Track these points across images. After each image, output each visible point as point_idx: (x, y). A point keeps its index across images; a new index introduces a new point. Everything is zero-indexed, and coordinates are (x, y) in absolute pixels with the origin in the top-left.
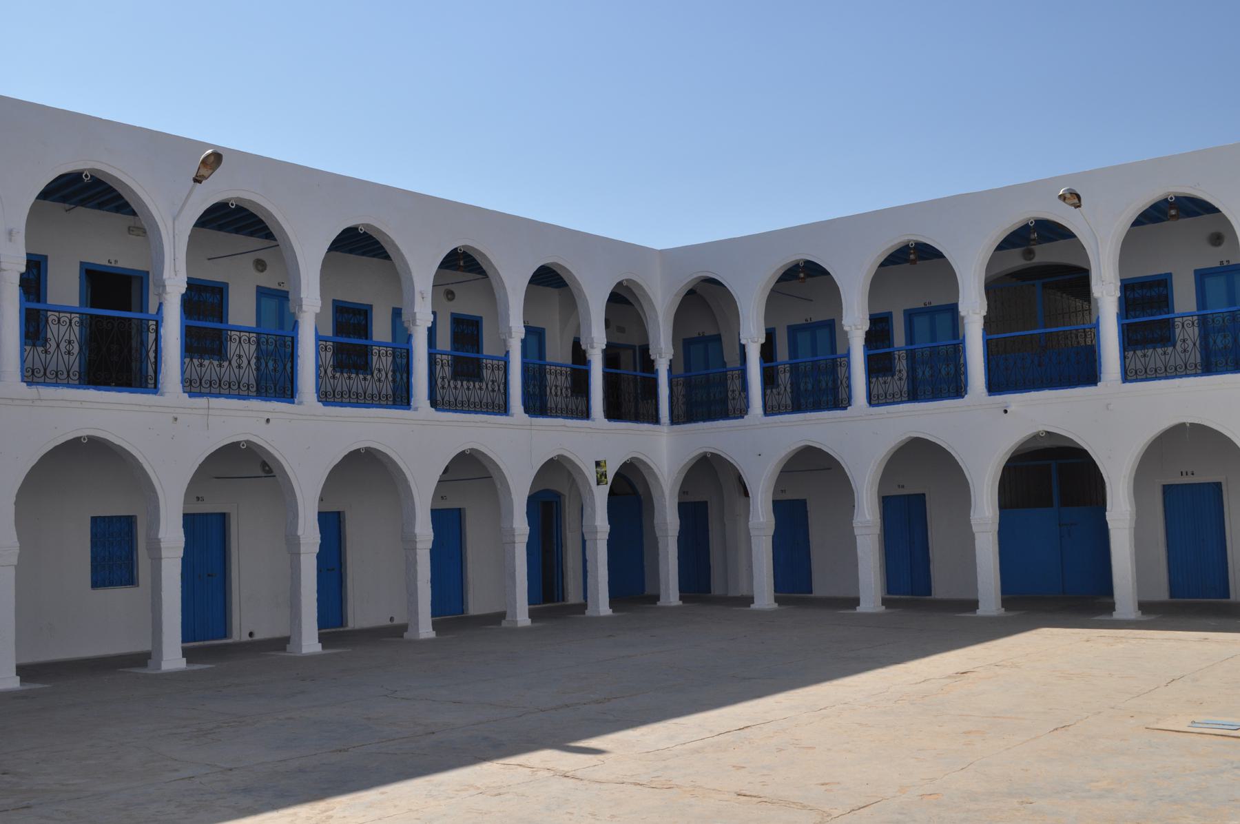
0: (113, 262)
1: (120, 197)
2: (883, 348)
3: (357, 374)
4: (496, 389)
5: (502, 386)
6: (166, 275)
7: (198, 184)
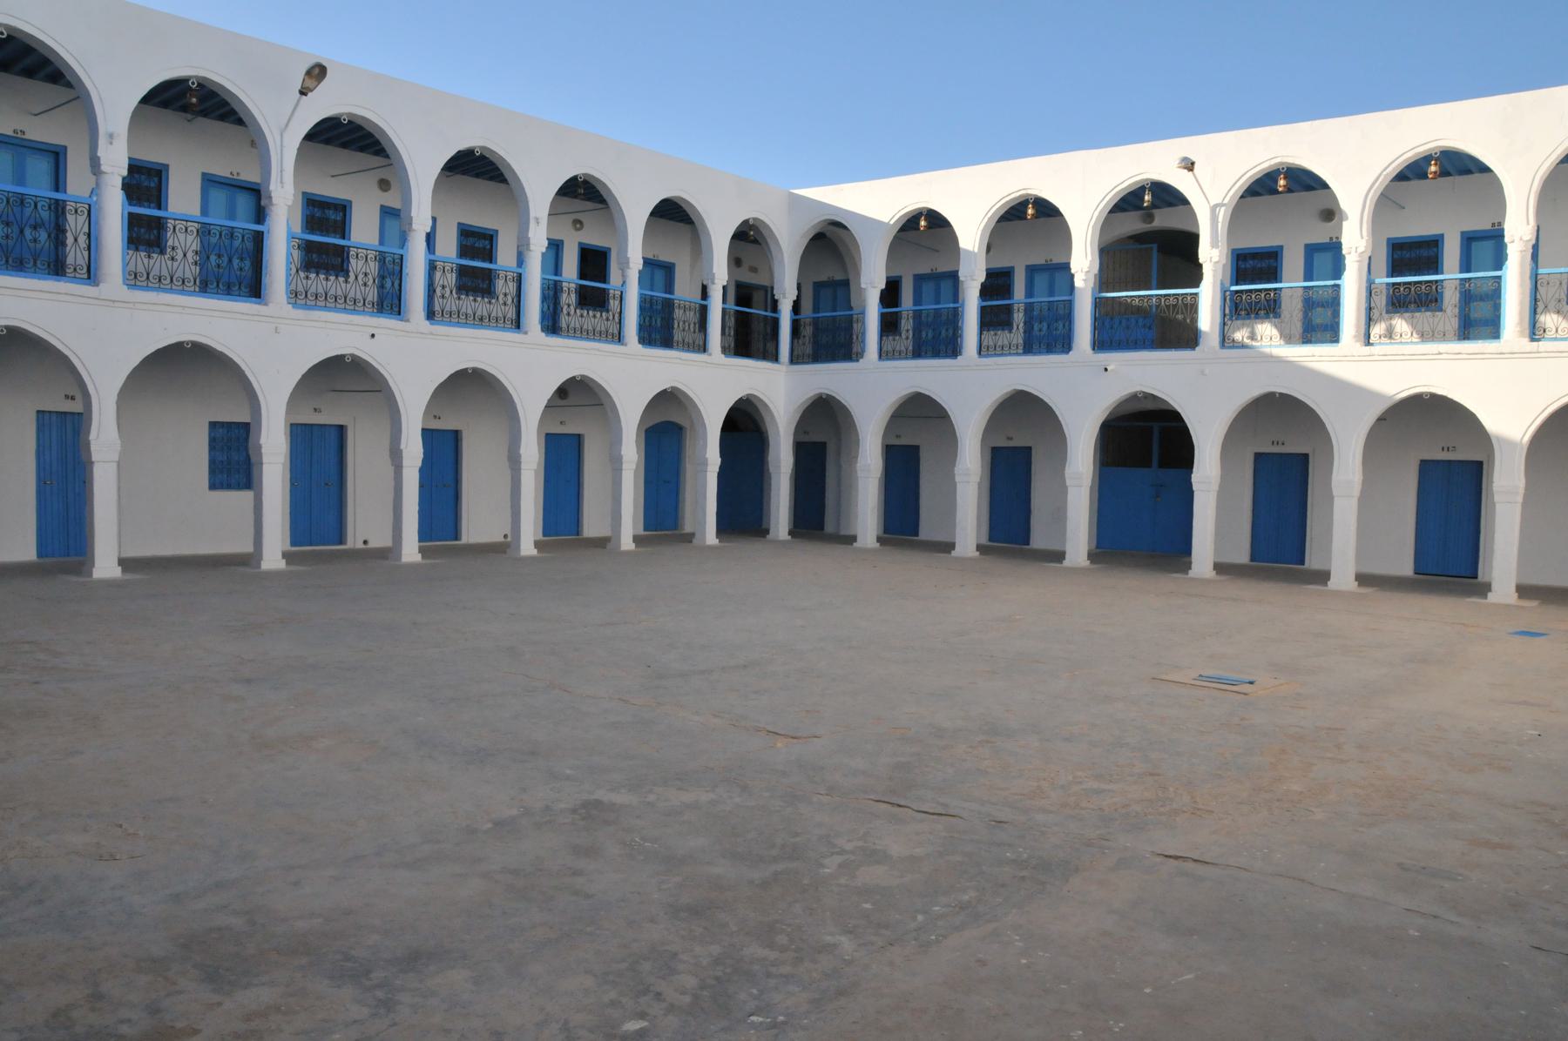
0: (235, 174)
3: (337, 277)
5: (617, 316)
6: (272, 187)
7: (304, 97)
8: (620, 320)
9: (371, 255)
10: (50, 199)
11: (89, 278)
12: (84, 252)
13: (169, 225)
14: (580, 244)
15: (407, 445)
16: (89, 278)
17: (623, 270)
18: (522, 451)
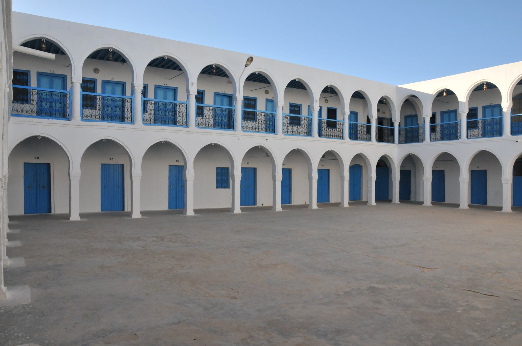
1: (224, 72)
2: (474, 119)
3: (250, 121)
4: (340, 131)
5: (342, 130)
6: (237, 95)
8: (343, 131)
9: (211, 108)
10: (162, 102)
11: (186, 125)
12: (98, 111)
13: (97, 98)
14: (327, 107)
15: (188, 172)
16: (186, 125)
17: (343, 115)
18: (313, 175)
